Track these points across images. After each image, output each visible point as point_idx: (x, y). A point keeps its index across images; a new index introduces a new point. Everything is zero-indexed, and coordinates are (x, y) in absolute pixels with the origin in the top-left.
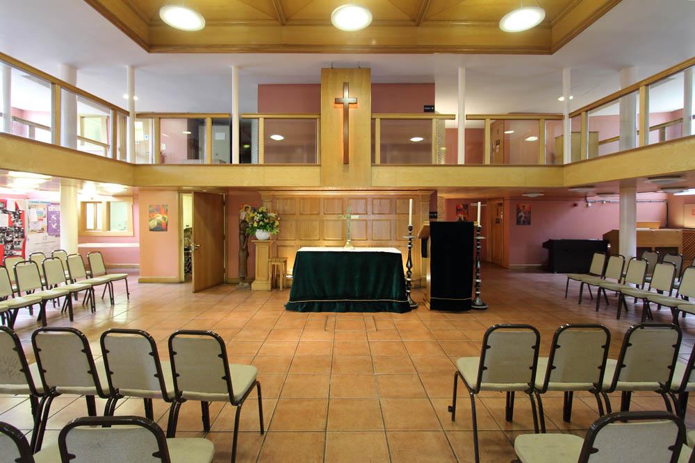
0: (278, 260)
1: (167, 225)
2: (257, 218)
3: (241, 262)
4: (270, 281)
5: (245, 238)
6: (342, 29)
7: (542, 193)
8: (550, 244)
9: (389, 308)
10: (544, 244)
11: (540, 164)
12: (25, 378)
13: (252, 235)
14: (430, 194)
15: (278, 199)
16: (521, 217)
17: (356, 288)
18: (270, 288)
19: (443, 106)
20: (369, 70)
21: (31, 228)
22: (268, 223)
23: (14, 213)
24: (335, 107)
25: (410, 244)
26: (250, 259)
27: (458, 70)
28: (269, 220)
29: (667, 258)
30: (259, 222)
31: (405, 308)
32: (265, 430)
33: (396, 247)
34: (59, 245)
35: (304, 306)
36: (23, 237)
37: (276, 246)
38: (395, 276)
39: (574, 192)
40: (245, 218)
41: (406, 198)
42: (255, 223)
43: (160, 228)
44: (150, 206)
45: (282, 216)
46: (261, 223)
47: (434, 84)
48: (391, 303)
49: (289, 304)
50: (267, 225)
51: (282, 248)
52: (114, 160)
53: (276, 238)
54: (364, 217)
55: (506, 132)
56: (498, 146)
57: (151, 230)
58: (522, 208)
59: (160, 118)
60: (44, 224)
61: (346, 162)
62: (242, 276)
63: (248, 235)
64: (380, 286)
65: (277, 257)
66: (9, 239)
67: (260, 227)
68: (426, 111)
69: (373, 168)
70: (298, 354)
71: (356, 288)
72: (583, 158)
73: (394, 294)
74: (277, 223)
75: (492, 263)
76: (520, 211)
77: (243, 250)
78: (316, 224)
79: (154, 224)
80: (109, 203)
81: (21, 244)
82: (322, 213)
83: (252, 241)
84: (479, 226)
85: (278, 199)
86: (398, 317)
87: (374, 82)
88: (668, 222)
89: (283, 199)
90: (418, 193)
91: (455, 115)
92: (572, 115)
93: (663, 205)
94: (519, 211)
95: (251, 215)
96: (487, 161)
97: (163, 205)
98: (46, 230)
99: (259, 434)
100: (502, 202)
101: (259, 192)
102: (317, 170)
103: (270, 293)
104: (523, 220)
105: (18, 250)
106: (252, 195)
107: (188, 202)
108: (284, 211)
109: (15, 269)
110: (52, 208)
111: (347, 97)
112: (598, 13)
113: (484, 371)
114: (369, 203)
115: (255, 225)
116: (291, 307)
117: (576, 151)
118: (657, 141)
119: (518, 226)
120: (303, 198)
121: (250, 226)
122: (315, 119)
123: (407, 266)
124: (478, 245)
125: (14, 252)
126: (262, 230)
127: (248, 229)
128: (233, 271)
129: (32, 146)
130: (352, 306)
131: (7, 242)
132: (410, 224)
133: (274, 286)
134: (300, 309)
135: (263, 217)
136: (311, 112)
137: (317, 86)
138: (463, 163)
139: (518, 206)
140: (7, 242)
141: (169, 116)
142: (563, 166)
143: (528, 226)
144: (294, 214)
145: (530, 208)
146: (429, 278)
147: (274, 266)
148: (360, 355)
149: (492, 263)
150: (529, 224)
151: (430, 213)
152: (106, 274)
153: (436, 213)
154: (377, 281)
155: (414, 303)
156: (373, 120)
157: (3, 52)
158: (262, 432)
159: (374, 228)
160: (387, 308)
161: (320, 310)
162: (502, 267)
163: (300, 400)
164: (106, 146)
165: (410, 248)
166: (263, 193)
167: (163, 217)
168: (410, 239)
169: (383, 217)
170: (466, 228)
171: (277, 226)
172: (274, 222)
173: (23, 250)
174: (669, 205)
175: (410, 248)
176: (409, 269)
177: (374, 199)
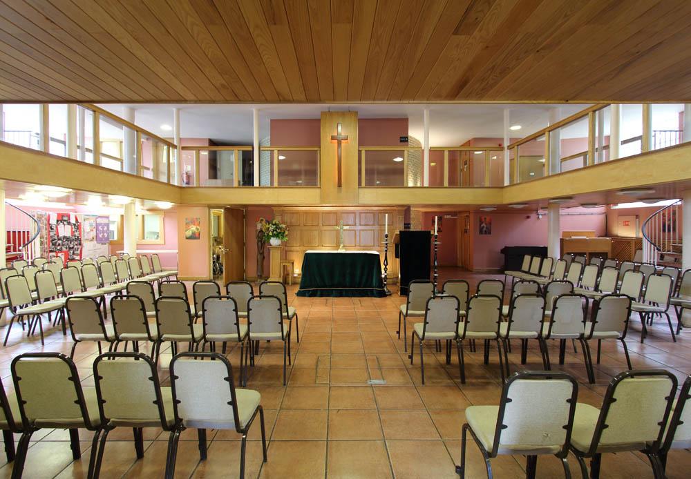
2: (271, 229)
3: (260, 263)
8: (506, 251)
10: (506, 248)
15: (287, 213)
19: (415, 134)
21: (85, 238)
22: (280, 233)
23: (75, 225)
24: (331, 143)
29: (578, 258)
31: (382, 294)
33: (378, 251)
36: (80, 244)
37: (285, 251)
39: (512, 208)
43: (194, 237)
44: (186, 219)
45: (290, 226)
46: (275, 232)
47: (408, 119)
49: (299, 291)
53: (285, 244)
54: (353, 228)
57: (187, 238)
58: (483, 220)
60: (93, 234)
61: (340, 185)
62: (259, 274)
63: (264, 242)
64: (365, 277)
65: (286, 259)
66: (71, 246)
67: (274, 236)
68: (401, 141)
72: (515, 183)
74: (287, 233)
76: (482, 223)
77: (261, 254)
78: (316, 233)
79: (189, 233)
80: (143, 216)
81: (79, 250)
84: (436, 234)
85: (287, 213)
86: (377, 300)
88: (606, 232)
89: (290, 213)
90: (395, 208)
93: (603, 217)
94: (481, 222)
95: (267, 226)
97: (197, 219)
98: (95, 238)
101: (273, 208)
102: (318, 191)
104: (485, 231)
105: (77, 255)
106: (267, 211)
108: (291, 222)
109: (61, 273)
110: (99, 221)
113: (427, 325)
115: (271, 234)
118: (582, 166)
119: (481, 235)
120: (306, 213)
124: (436, 248)
125: (75, 256)
129: (81, 166)
131: (70, 248)
132: (386, 233)
135: (276, 227)
136: (312, 145)
137: (319, 121)
138: (427, 186)
140: (70, 248)
142: (503, 187)
143: (489, 235)
146: (400, 276)
149: (462, 267)
150: (490, 233)
152: (162, 271)
155: (389, 292)
156: (360, 152)
158: (298, 342)
161: (321, 296)
162: (471, 271)
164: (121, 161)
168: (386, 244)
170: (426, 236)
173: (81, 255)
174: (607, 216)
175: (386, 251)
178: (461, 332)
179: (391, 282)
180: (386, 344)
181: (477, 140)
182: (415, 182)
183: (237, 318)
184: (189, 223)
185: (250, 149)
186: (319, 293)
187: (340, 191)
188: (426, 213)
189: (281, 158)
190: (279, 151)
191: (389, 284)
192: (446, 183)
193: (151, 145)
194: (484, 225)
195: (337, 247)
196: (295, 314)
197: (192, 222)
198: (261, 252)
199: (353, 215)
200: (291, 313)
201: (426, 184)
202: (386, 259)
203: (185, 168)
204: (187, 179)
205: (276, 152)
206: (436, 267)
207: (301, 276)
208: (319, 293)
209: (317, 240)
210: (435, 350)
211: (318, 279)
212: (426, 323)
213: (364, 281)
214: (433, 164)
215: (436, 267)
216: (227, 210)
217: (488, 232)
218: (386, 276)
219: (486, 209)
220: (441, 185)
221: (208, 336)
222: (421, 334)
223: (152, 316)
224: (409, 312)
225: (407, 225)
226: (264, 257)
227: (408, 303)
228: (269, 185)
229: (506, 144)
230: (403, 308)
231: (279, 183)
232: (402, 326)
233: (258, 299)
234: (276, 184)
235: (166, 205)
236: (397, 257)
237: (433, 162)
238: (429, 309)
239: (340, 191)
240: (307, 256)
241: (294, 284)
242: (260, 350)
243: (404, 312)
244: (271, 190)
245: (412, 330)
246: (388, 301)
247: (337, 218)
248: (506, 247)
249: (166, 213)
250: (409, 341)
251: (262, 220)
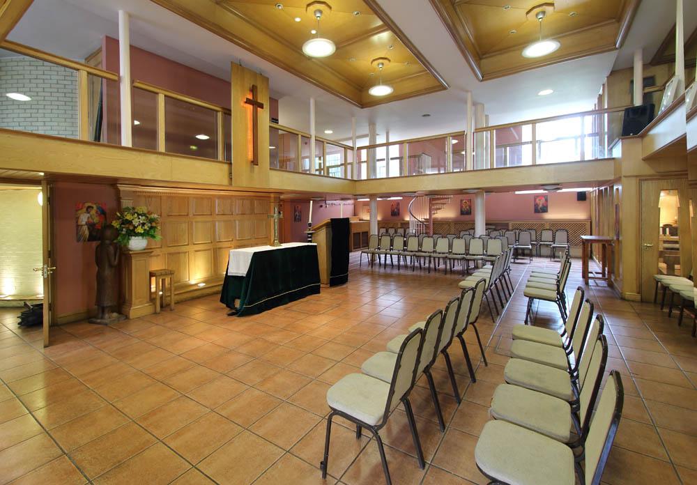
6: (385, 96)
78: (184, 226)
82: (191, 215)
87: (109, 35)
94: (295, 211)
96: (126, 139)
112: (354, 41)
120: (171, 197)
157: (34, 3)
192: (126, 139)
194: (297, 213)
214: (136, 123)
237: (137, 120)
239: (252, 170)
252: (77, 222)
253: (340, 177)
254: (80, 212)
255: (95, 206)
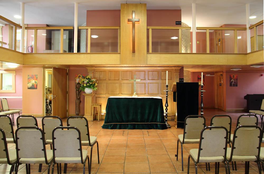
0: (97, 104)
1: (37, 86)
3: (77, 105)
4: (92, 116)
5: (79, 92)
7: (240, 68)
8: (248, 97)
9: (156, 127)
11: (235, 53)
12: (12, 135)
13: (83, 91)
14: (179, 69)
16: (232, 82)
17: (139, 117)
18: (92, 119)
19: (186, 20)
20: (145, 4)
22: (91, 84)
25: (167, 94)
26: (81, 105)
27: (192, 4)
28: (92, 83)
30: (87, 83)
31: (164, 127)
32: (100, 163)
33: (161, 97)
34: (251, 31)
35: (112, 126)
37: (95, 96)
38: (159, 111)
40: (79, 82)
41: (165, 71)
42: (85, 84)
43: (34, 87)
45: (99, 80)
47: (181, 10)
48: (157, 124)
50: (91, 85)
51: (98, 98)
52: (15, 51)
53: (95, 93)
55: (225, 35)
56: (219, 42)
57: (29, 88)
59: (37, 29)
61: (134, 51)
62: (77, 113)
63: (81, 91)
65: (96, 103)
67: (87, 87)
68: (176, 24)
69: (148, 55)
70: (110, 143)
71: (139, 117)
73: (158, 121)
74: (96, 84)
75: (218, 109)
77: (78, 99)
78: (117, 85)
79: (30, 85)
82: (120, 79)
83: (83, 94)
84: (202, 85)
89: (103, 71)
90: (173, 68)
91: (191, 27)
92: (251, 28)
94: (231, 79)
95: (83, 80)
96: (208, 51)
97: (35, 75)
99: (98, 164)
100: (222, 74)
101: (87, 68)
102: (118, 55)
103: (93, 122)
106: (83, 70)
107: (48, 73)
108: (100, 78)
111: (134, 17)
113: (185, 134)
114: (147, 73)
115: (85, 85)
116: (105, 127)
117: (252, 47)
119: (231, 87)
120: (110, 71)
121: (82, 86)
122: (117, 29)
123: (165, 106)
124: (202, 94)
126: (88, 88)
127: (80, 88)
128: (72, 110)
130: (136, 126)
132: (167, 84)
133: (95, 119)
134: (110, 127)
135: (89, 81)
139: (230, 76)
141: (42, 28)
142: (247, 54)
144: (105, 80)
145: (237, 77)
146: (177, 114)
147: (94, 107)
148: (140, 143)
150: (237, 86)
151: (180, 79)
152: (9, 110)
153: (183, 79)
154: (149, 113)
155: (169, 125)
156: (148, 30)
159: (149, 88)
160: (155, 128)
163: (113, 156)
165: (167, 96)
166: (88, 68)
167: (35, 82)
168: (167, 92)
169: (154, 81)
170: (195, 86)
171: (96, 86)
172: (95, 84)
176: (167, 107)
177: (149, 71)
178: (228, 156)
179: (170, 119)
180: (167, 165)
181: (226, 25)
182: (186, 50)
183: (81, 145)
184: (30, 78)
185: (72, 28)
186: (118, 126)
187: (134, 56)
188: (193, 73)
189: (95, 37)
190: (91, 29)
191: (169, 120)
192: (208, 51)
193: (8, 28)
194: (232, 80)
195: (132, 94)
196: (96, 142)
197: (32, 78)
198: (79, 98)
199: (144, 72)
200: (92, 141)
201: (194, 51)
202: (167, 102)
203: (30, 43)
204: (31, 50)
205: (89, 31)
206: (202, 108)
207: (105, 115)
208: (118, 126)
209: (118, 90)
210: (206, 169)
211: (118, 117)
212: (200, 149)
213: (151, 118)
214: (198, 42)
215: (202, 108)
216: (55, 69)
217: (236, 85)
218: (167, 114)
219: (234, 70)
220: (204, 52)
221: (22, 159)
222: (196, 158)
223: (10, 142)
224: (185, 140)
225: (181, 79)
226: (80, 102)
227: (185, 133)
228: (85, 52)
229: (248, 27)
230: (181, 137)
231: (91, 51)
232: (180, 150)
233: (67, 129)
234: (89, 51)
235: (14, 66)
236: (174, 101)
237: (198, 41)
238: (203, 138)
239: (134, 56)
240: (110, 100)
241: (101, 120)
242: (67, 169)
243: (181, 140)
244: (85, 55)
245: (189, 154)
246: (168, 132)
247: (132, 74)
248: (248, 95)
249: (16, 71)
250: (186, 162)
251: (80, 76)
252: (75, 82)
253: (237, 53)
254: (76, 78)
255: (81, 76)
